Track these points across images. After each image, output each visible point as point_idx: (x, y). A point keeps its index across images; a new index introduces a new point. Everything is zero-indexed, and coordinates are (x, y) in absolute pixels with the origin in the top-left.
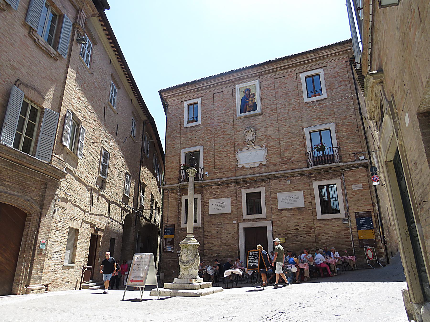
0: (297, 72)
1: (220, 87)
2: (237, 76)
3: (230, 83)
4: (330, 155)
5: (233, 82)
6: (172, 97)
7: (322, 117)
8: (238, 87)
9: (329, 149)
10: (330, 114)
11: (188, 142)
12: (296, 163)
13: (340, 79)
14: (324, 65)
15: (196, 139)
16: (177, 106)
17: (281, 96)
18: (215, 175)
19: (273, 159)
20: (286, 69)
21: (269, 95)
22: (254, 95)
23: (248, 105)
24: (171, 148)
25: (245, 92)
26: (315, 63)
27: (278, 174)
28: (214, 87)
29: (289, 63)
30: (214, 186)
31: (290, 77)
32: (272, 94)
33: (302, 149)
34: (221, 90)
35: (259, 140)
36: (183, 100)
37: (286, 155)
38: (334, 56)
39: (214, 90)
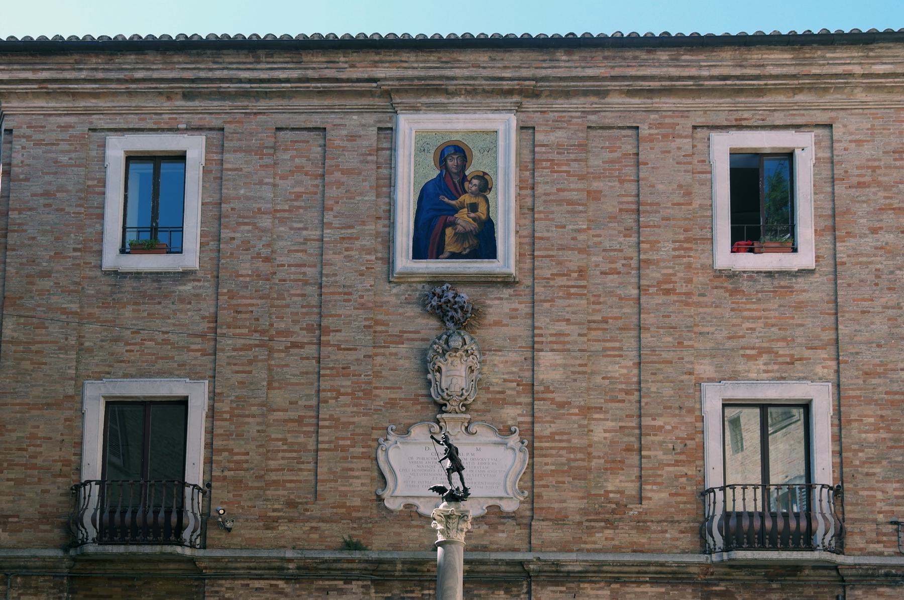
0: (700, 121)
1: (316, 102)
2: (415, 67)
3: (371, 94)
4: (751, 515)
5: (387, 94)
6: (36, 95)
7: (782, 349)
8: (412, 126)
9: (739, 490)
10: (817, 343)
11: (120, 348)
12: (654, 527)
13: (880, 197)
14: (822, 118)
15: (166, 342)
16: (64, 146)
17: (612, 218)
18: (268, 528)
19: (555, 495)
20: (651, 92)
21: (559, 202)
22: (485, 185)
23: (453, 224)
24: (26, 365)
25: (442, 160)
26: (781, 98)
27: (572, 560)
28: (282, 94)
29: (674, 72)
30: (260, 578)
31: (665, 136)
32: (574, 196)
33: (684, 470)
34: (316, 121)
35: (495, 402)
36: (99, 121)
37: (613, 483)
38: (869, 88)
39: (276, 112)
